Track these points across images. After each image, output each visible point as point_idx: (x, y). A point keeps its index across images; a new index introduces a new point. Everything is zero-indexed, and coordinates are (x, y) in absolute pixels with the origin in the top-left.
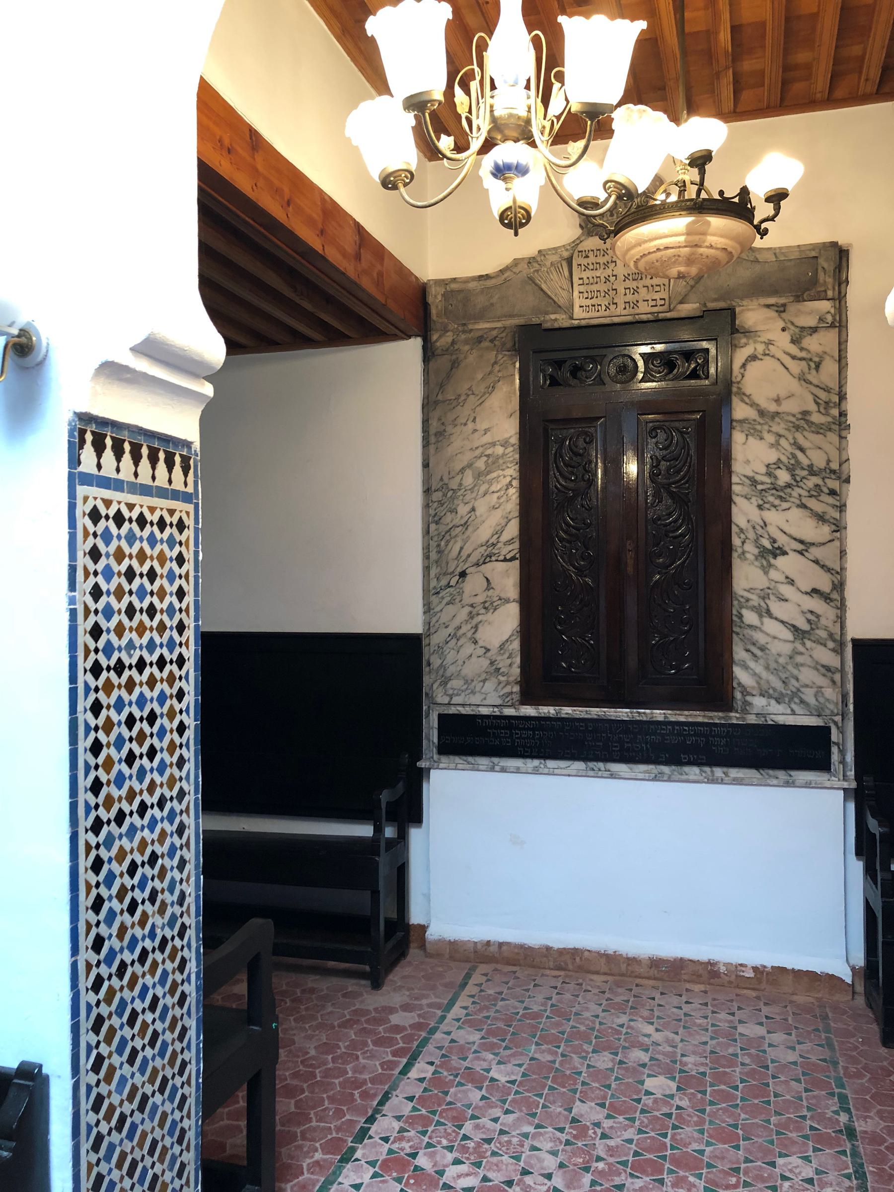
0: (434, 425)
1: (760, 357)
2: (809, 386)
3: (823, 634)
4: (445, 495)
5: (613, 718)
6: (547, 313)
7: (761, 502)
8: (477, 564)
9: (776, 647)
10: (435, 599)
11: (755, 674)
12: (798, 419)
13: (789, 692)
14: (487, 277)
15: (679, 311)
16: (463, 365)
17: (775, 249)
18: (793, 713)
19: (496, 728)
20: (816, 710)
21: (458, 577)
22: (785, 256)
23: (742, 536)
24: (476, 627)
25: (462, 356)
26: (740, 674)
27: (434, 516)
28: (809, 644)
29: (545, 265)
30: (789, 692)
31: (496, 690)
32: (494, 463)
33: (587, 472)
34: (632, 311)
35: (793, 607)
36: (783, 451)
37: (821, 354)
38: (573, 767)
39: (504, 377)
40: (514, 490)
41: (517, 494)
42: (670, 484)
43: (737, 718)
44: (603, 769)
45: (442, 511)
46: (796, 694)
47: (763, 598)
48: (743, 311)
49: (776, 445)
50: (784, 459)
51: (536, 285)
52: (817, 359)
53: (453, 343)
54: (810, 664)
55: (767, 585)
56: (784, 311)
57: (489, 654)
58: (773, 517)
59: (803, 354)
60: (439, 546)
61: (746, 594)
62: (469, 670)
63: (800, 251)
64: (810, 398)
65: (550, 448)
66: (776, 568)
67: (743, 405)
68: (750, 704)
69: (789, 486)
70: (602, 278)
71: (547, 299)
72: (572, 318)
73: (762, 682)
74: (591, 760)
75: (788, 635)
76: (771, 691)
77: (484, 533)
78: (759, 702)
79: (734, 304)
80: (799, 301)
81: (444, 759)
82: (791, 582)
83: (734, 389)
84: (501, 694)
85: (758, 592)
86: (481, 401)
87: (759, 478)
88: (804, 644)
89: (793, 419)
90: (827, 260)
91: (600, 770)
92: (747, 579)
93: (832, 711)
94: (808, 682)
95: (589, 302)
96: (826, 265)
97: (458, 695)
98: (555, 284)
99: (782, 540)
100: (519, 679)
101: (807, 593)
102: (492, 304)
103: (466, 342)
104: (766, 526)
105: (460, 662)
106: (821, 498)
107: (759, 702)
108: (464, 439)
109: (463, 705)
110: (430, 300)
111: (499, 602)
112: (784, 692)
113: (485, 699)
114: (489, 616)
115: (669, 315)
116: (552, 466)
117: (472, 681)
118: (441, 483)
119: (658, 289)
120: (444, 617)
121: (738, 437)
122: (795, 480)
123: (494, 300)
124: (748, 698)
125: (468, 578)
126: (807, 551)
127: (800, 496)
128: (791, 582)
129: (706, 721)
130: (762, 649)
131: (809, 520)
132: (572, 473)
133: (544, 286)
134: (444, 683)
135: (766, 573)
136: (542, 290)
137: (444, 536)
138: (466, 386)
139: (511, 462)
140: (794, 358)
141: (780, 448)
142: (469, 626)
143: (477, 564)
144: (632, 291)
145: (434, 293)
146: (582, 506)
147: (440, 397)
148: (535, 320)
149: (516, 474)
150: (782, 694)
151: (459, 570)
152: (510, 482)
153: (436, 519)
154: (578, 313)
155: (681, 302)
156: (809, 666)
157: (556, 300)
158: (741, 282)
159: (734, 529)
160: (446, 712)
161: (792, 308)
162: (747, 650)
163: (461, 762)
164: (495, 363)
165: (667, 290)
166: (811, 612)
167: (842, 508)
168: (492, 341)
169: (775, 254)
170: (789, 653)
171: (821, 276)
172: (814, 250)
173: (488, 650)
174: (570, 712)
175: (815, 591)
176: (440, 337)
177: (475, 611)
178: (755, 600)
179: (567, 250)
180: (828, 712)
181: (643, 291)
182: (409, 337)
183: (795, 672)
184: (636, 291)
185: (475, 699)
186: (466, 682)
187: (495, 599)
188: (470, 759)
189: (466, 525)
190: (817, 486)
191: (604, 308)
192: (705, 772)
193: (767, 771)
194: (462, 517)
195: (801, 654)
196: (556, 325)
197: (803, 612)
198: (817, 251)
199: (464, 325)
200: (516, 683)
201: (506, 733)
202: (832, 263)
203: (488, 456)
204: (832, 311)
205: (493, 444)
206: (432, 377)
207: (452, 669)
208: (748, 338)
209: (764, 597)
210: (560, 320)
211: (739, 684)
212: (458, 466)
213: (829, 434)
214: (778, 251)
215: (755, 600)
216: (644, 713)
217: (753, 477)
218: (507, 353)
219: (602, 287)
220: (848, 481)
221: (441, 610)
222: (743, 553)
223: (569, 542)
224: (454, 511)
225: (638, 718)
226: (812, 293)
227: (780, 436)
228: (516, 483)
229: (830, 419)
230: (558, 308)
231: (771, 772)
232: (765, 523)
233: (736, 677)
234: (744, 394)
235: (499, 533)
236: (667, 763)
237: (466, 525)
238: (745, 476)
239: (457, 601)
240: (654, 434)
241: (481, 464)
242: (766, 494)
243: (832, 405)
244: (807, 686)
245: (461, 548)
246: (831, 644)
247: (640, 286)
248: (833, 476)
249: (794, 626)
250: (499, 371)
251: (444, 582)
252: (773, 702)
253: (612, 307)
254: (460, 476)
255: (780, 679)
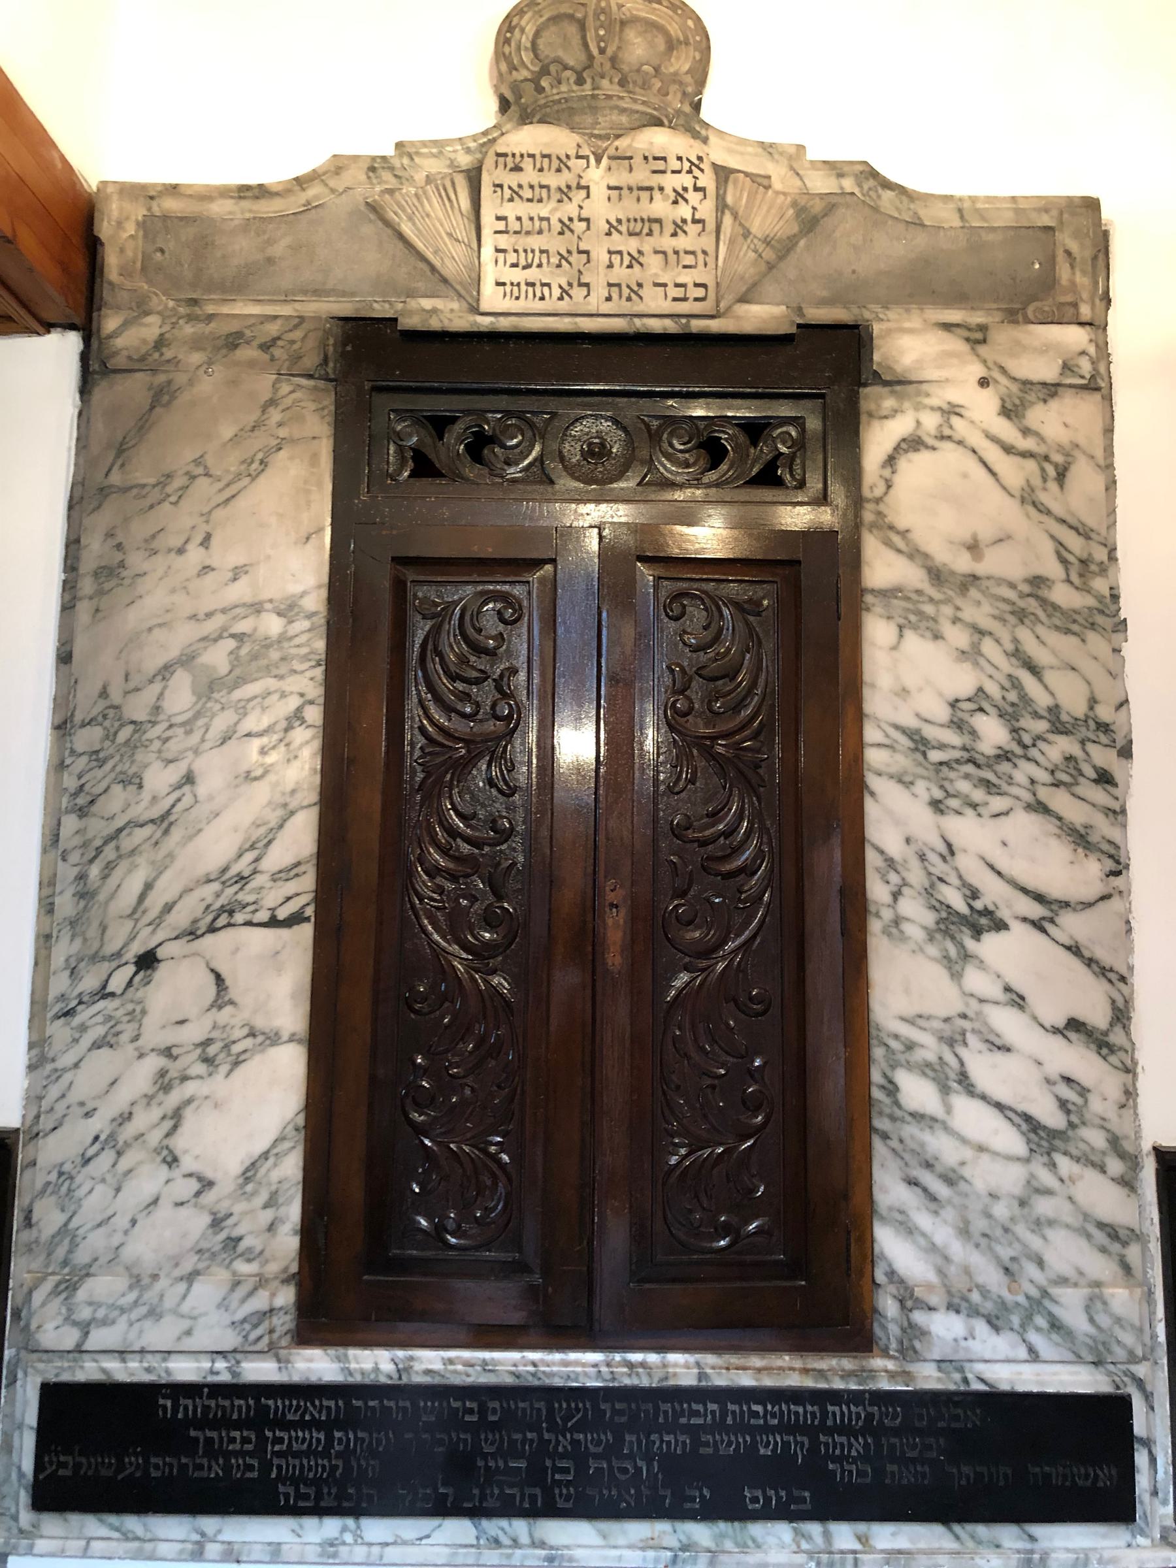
0: (95, 548)
1: (930, 441)
2: (1044, 518)
3: (1096, 1138)
4: (110, 736)
5: (558, 1382)
6: (412, 294)
7: (938, 794)
8: (192, 934)
9: (986, 1175)
10: (59, 1031)
11: (932, 1248)
12: (1022, 596)
13: (1021, 1299)
14: (261, 192)
15: (738, 318)
16: (184, 398)
17: (961, 199)
18: (1034, 1356)
19: (215, 1424)
20: (1092, 1349)
21: (132, 969)
22: (984, 219)
23: (894, 878)
24: (176, 1117)
25: (181, 378)
26: (894, 1249)
27: (75, 795)
28: (1065, 1164)
29: (411, 180)
30: (1021, 1299)
31: (223, 1305)
32: (254, 657)
33: (505, 696)
34: (626, 307)
35: (1024, 1067)
36: (990, 670)
37: (1068, 446)
38: (439, 1537)
39: (292, 441)
40: (308, 734)
41: (317, 744)
42: (714, 738)
43: (892, 1376)
44: (524, 1539)
45: (98, 779)
46: (1039, 1303)
47: (951, 1043)
48: (889, 331)
49: (971, 655)
50: (993, 689)
51: (387, 223)
52: (1058, 458)
53: (160, 343)
54: (1069, 1220)
55: (958, 1006)
56: (984, 341)
57: (209, 1197)
58: (968, 831)
59: (1028, 444)
60: (82, 877)
61: (905, 1030)
62: (147, 1245)
63: (1017, 211)
64: (1048, 547)
65: (402, 640)
66: (981, 964)
67: (890, 555)
68: (923, 1333)
69: (1004, 756)
70: (554, 221)
71: (412, 260)
72: (475, 310)
73: (952, 1270)
74: (490, 1514)
75: (1011, 1140)
76: (975, 1297)
77: (215, 846)
78: (944, 1328)
79: (867, 315)
80: (1016, 322)
81: (52, 1524)
82: (1018, 1001)
83: (868, 516)
84: (239, 1316)
85: (937, 1024)
86: (228, 493)
87: (930, 732)
88: (1053, 1166)
89: (1011, 595)
90: (1076, 235)
91: (516, 1543)
92: (907, 991)
93: (1131, 1353)
94: (1066, 1270)
95: (518, 275)
96: (1074, 246)
97: (105, 1322)
98: (436, 226)
99: (994, 892)
100: (294, 1268)
101: (1056, 1031)
102: (270, 261)
103: (196, 344)
104: (952, 853)
105: (122, 1222)
106: (1079, 790)
107: (944, 1328)
108: (173, 591)
109: (122, 1354)
110: (104, 230)
111: (248, 1043)
112: (1005, 1294)
113: (188, 1333)
114: (218, 1085)
115: (715, 326)
116: (414, 674)
117: (155, 1277)
118: (101, 705)
119: (689, 259)
120: (85, 1084)
121: (878, 632)
122: (1020, 743)
123: (278, 250)
124: (919, 1317)
125: (162, 972)
126: (1052, 921)
127: (1033, 782)
128: (1018, 1001)
129: (809, 1383)
130: (951, 1179)
131: (1054, 843)
132: (466, 697)
133: (407, 229)
134: (68, 1287)
135: (956, 976)
136: (401, 237)
137: (99, 851)
138: (189, 455)
139: (305, 658)
140: (1008, 449)
141: (982, 661)
142: (156, 1113)
143: (192, 934)
144: (627, 259)
145: (115, 214)
146: (491, 782)
147: (115, 478)
148: (381, 310)
149: (316, 691)
150: (1003, 1304)
151: (137, 948)
152: (299, 710)
153: (81, 800)
154: (491, 298)
155: (744, 299)
156: (1068, 1226)
157: (437, 262)
158: (882, 266)
159: (871, 857)
160: (66, 1377)
161: (1003, 336)
162: (912, 1182)
163: (103, 1531)
164: (272, 402)
165: (711, 265)
166: (1068, 1080)
167: (1118, 814)
168: (265, 347)
169: (960, 211)
170: (1018, 1190)
171: (1064, 272)
172: (1047, 211)
173: (207, 1184)
174: (438, 1366)
175: (1075, 1025)
176: (126, 324)
177: (175, 1068)
178: (930, 1048)
179: (468, 151)
180: (1120, 1354)
181: (654, 263)
182: (48, 327)
183: (1035, 1242)
184: (635, 260)
185: (158, 1335)
186: (136, 1282)
187: (238, 1033)
188: (132, 1522)
189: (164, 822)
190: (1069, 759)
191: (556, 292)
192: (809, 1538)
193: (970, 1527)
194: (154, 799)
195: (1048, 1192)
196: (435, 324)
197: (1048, 1081)
198: (1055, 213)
199: (194, 302)
200: (286, 1281)
201: (246, 1440)
202: (1088, 242)
203: (240, 637)
204: (1092, 350)
205: (256, 608)
206: (99, 426)
207: (94, 1243)
208: (901, 397)
209: (952, 1041)
210: (448, 314)
211: (892, 1274)
212: (153, 661)
213: (1091, 636)
214: (966, 205)
215: (930, 1048)
216: (643, 1364)
217: (918, 731)
218: (304, 382)
219: (555, 244)
220: (1126, 752)
221: (76, 1065)
222: (897, 921)
223: (454, 878)
224: (135, 781)
225: (627, 1381)
226: (1047, 305)
227: (982, 633)
228: (314, 714)
229: (1091, 601)
230: (442, 282)
231: (981, 1530)
232: (949, 846)
233: (883, 1257)
234: (891, 527)
235: (259, 845)
236: (707, 1513)
237: (164, 822)
238: (897, 727)
239: (125, 1038)
240: (676, 609)
241: (218, 658)
242: (952, 775)
243: (1093, 567)
244: (1063, 1281)
245: (148, 887)
246: (1115, 1166)
247: (646, 248)
248: (1104, 739)
249: (1028, 1118)
250: (280, 425)
251: (90, 982)
252: (981, 1327)
253: (578, 293)
254: (157, 687)
255: (998, 1259)
